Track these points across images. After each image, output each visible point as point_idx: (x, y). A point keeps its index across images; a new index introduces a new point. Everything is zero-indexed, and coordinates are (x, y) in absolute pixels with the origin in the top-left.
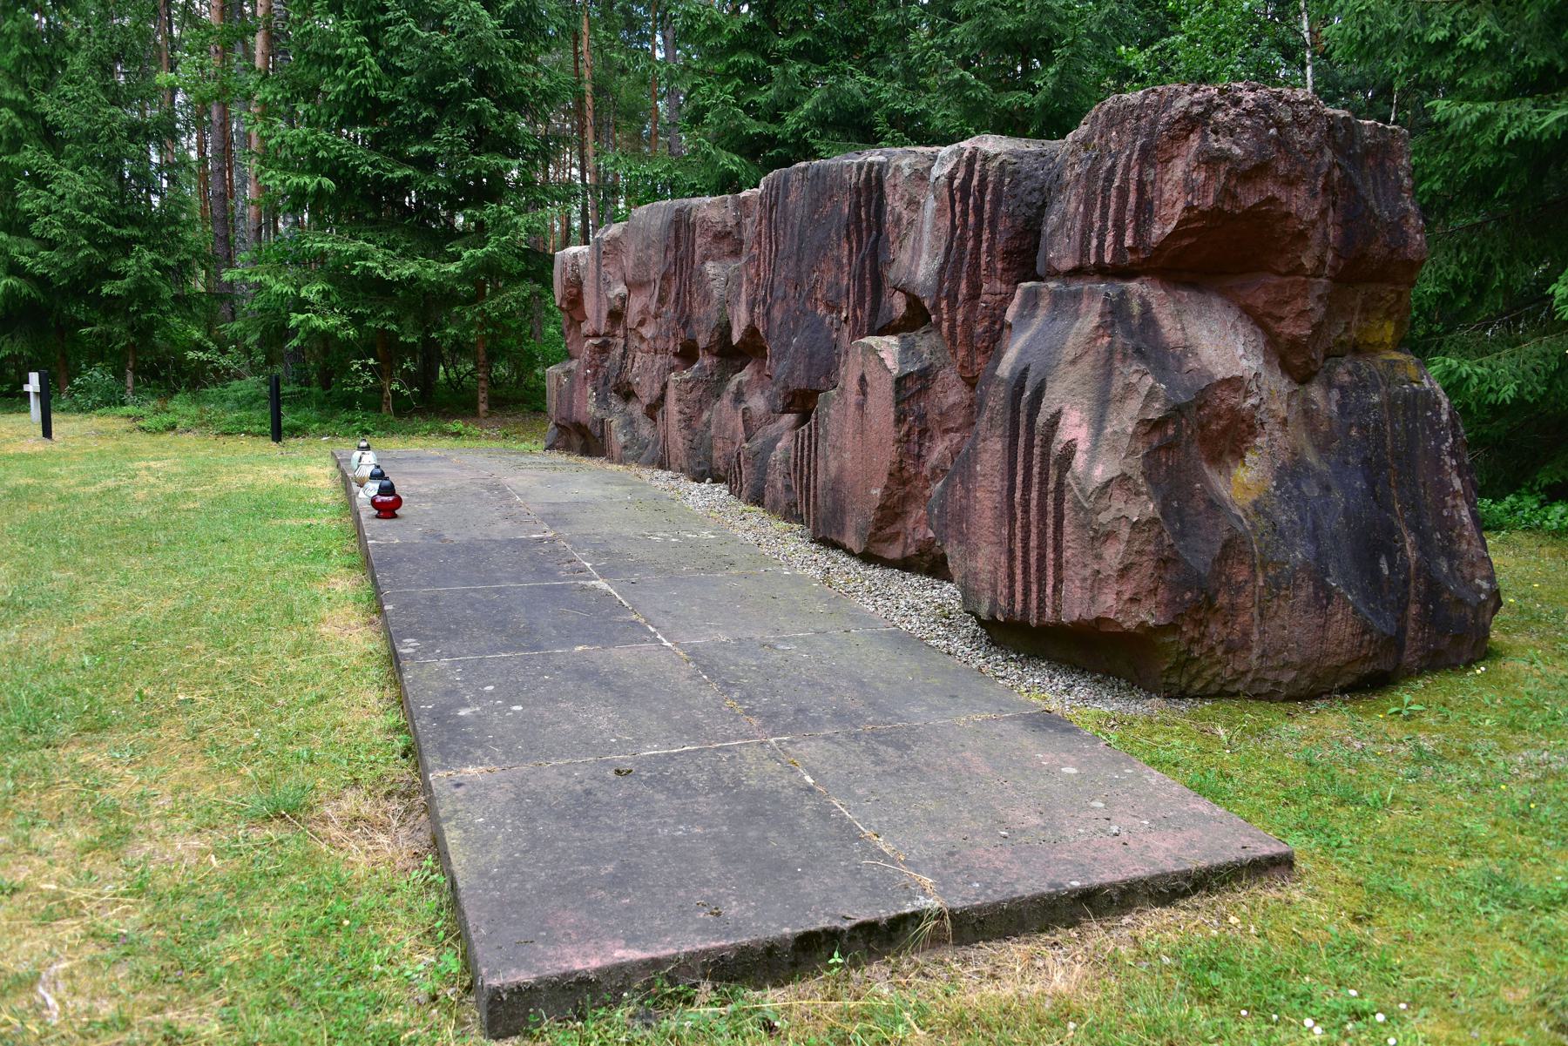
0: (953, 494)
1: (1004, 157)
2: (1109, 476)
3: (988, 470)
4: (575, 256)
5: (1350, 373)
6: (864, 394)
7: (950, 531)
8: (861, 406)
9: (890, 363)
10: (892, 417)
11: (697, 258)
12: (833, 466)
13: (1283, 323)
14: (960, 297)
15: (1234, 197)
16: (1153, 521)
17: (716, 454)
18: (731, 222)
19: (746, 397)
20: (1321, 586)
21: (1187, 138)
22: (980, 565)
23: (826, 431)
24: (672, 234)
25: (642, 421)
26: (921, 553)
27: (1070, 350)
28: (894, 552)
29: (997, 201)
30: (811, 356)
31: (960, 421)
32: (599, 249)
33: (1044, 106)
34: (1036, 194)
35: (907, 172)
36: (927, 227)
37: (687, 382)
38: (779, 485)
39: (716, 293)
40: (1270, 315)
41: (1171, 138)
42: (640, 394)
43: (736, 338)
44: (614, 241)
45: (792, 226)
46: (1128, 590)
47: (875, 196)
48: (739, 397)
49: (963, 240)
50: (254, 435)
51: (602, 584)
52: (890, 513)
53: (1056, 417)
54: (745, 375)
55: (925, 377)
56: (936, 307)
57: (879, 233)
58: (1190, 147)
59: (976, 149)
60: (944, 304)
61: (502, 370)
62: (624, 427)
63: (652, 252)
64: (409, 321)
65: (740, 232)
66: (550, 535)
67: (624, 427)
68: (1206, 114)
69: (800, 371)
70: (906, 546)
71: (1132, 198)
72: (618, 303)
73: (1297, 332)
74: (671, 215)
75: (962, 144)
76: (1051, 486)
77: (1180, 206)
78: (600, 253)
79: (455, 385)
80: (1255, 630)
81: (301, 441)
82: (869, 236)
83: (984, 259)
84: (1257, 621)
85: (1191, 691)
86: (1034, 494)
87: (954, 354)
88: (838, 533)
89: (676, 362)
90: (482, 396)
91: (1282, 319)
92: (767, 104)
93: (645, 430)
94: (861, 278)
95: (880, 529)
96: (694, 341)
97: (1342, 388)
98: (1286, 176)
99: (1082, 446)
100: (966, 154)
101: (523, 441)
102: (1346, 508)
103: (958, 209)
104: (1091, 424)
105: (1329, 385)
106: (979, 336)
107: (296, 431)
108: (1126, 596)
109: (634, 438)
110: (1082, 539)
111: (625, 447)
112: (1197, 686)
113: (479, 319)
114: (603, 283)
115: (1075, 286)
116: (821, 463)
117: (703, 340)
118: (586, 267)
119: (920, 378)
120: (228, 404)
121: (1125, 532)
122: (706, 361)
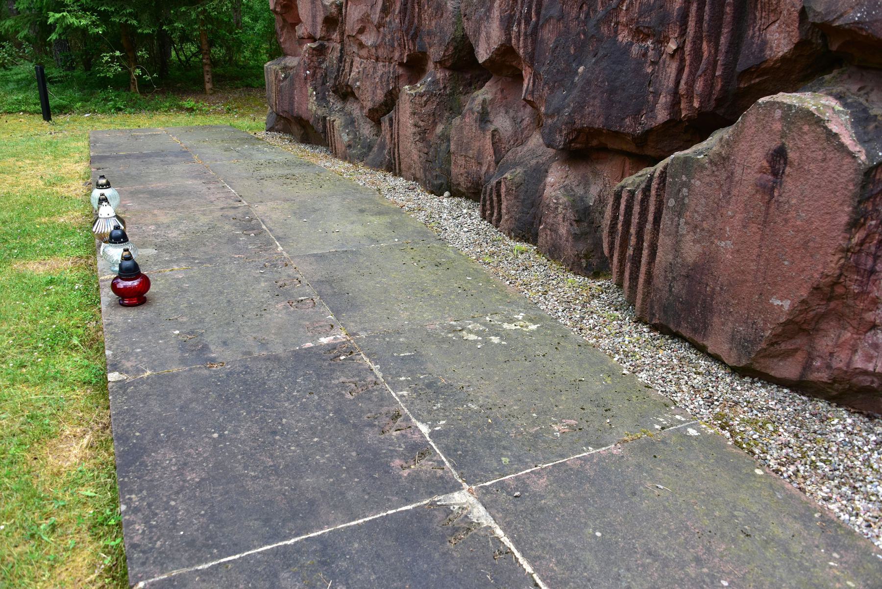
6: (776, 173)
12: (691, 251)
17: (455, 170)
19: (491, 117)
25: (361, 121)
28: (789, 369)
30: (612, 91)
37: (421, 95)
38: (563, 231)
43: (483, 55)
48: (484, 118)
50: (31, 113)
54: (486, 93)
61: (218, 52)
62: (346, 127)
64: (145, 17)
66: (341, 336)
67: (346, 127)
70: (807, 367)
72: (334, 10)
79: (186, 66)
81: (68, 118)
89: (400, 71)
90: (207, 77)
93: (366, 130)
95: (772, 344)
101: (243, 115)
107: (63, 110)
109: (356, 137)
111: (349, 146)
113: (201, 17)
116: (664, 240)
117: (435, 53)
120: (11, 86)
122: (434, 74)
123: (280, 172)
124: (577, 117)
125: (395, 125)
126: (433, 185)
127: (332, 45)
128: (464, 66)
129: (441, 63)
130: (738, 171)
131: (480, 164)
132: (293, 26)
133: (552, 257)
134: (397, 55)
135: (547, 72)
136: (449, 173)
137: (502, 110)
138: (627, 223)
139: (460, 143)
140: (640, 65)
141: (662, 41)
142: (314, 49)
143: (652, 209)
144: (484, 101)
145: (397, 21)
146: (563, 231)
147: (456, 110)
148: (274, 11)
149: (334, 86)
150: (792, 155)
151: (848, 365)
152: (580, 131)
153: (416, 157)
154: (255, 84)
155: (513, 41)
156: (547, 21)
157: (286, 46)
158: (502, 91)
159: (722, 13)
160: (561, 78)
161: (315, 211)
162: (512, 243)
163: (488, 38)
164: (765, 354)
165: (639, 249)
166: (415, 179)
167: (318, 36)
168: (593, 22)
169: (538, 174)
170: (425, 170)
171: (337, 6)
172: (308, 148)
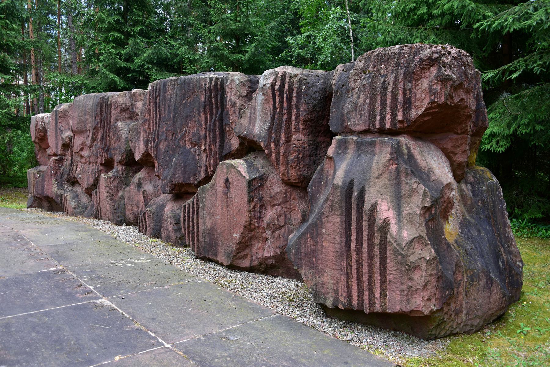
0: (305, 243)
1: (301, 76)
2: (412, 237)
3: (330, 232)
4: (43, 118)
5: (473, 177)
6: (228, 188)
7: (303, 261)
8: (226, 194)
9: (244, 173)
10: (246, 199)
11: (113, 120)
12: (209, 223)
13: (457, 156)
14: (281, 142)
15: (452, 98)
16: (435, 258)
17: (127, 212)
18: (129, 104)
19: (143, 185)
20: (489, 278)
21: (429, 69)
22: (326, 280)
23: (204, 205)
24: (99, 109)
25: (82, 195)
26: (260, 264)
27: (375, 170)
28: (245, 263)
29: (299, 97)
30: (185, 167)
31: (281, 200)
32: (56, 115)
33: (249, 60)
34: (317, 94)
35: (237, 82)
36: (259, 108)
37: (110, 178)
38: (170, 229)
39: (123, 136)
40: (452, 152)
41: (421, 69)
42: (81, 183)
43: (137, 157)
44: (65, 112)
45: (169, 106)
46: (426, 294)
47: (220, 93)
48: (139, 185)
49: (281, 114)
51: (105, 301)
52: (244, 245)
53: (374, 207)
54: (141, 174)
55: (262, 179)
56: (268, 146)
57: (223, 110)
58: (430, 74)
59: (285, 72)
60: (273, 145)
62: (73, 198)
63: (87, 117)
65: (132, 108)
66: (60, 267)
67: (73, 198)
68: (439, 58)
69: (179, 174)
70: (252, 261)
71: (400, 97)
72: (68, 140)
73: (462, 160)
74: (99, 100)
75: (277, 69)
76: (377, 242)
77: (426, 102)
78: (63, 117)
80: (464, 303)
82: (217, 112)
83: (293, 124)
84: (465, 298)
85: (439, 336)
86: (365, 246)
87: (278, 169)
88: (214, 255)
89: (101, 168)
91: (457, 154)
92: (126, 54)
93: (85, 199)
94: (214, 131)
95: (238, 253)
96: (112, 158)
97: (471, 183)
98: (467, 89)
99: (393, 221)
100: (280, 75)
101: (12, 202)
102: (488, 240)
103: (277, 99)
104: (394, 210)
105: (466, 183)
106: (292, 160)
108: (426, 298)
109: (79, 203)
110: (400, 270)
111: (75, 208)
112: (442, 333)
114: (58, 131)
115: (368, 138)
116: (201, 221)
117: (117, 158)
118: (49, 123)
119: (260, 180)
121: (424, 265)
122: (118, 168)
123: (34, 221)
124: (173, 179)
125: (98, 194)
126: (117, 221)
127: (66, 158)
128: (131, 164)
129: (120, 162)
130: (218, 188)
131: (138, 207)
132: (45, 149)
133: (167, 242)
134: (99, 160)
135: (162, 162)
136: (125, 214)
137: (149, 182)
138: (189, 217)
139: (129, 199)
140: (194, 156)
141: (200, 146)
142: (56, 160)
143: (195, 209)
144: (139, 178)
145: (99, 144)
146: (170, 229)
147: (127, 185)
148: (35, 142)
149: (67, 178)
150: (230, 180)
151: (262, 256)
152: (175, 185)
153: (108, 208)
154: (21, 185)
155: (149, 150)
156: (161, 141)
157: (41, 160)
158: (148, 173)
159: (216, 134)
160: (167, 164)
161: (52, 231)
162: (151, 239)
163: (139, 149)
164: (235, 258)
165: (193, 227)
166: (109, 220)
167: (59, 153)
168: (177, 141)
169: (163, 206)
170: (113, 214)
171: (69, 138)
172: (52, 214)
